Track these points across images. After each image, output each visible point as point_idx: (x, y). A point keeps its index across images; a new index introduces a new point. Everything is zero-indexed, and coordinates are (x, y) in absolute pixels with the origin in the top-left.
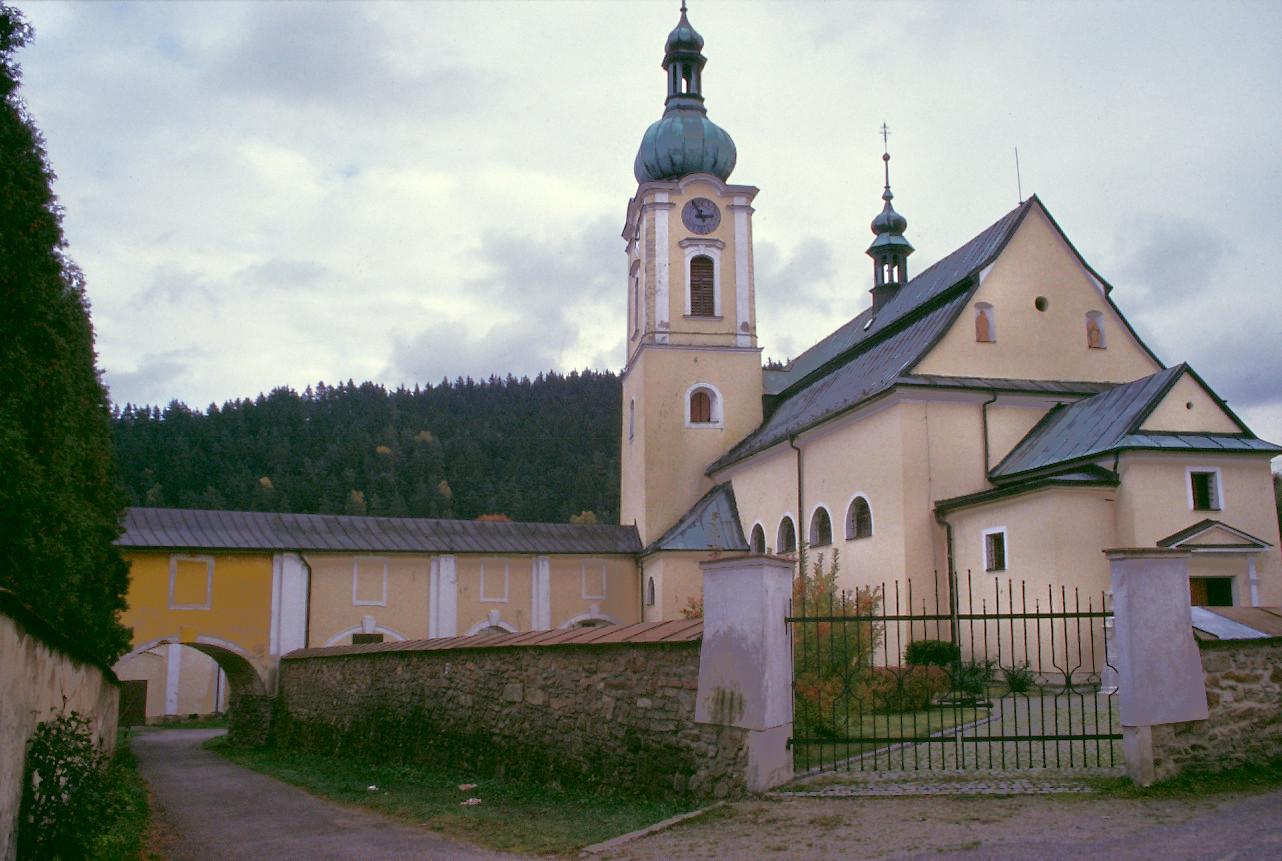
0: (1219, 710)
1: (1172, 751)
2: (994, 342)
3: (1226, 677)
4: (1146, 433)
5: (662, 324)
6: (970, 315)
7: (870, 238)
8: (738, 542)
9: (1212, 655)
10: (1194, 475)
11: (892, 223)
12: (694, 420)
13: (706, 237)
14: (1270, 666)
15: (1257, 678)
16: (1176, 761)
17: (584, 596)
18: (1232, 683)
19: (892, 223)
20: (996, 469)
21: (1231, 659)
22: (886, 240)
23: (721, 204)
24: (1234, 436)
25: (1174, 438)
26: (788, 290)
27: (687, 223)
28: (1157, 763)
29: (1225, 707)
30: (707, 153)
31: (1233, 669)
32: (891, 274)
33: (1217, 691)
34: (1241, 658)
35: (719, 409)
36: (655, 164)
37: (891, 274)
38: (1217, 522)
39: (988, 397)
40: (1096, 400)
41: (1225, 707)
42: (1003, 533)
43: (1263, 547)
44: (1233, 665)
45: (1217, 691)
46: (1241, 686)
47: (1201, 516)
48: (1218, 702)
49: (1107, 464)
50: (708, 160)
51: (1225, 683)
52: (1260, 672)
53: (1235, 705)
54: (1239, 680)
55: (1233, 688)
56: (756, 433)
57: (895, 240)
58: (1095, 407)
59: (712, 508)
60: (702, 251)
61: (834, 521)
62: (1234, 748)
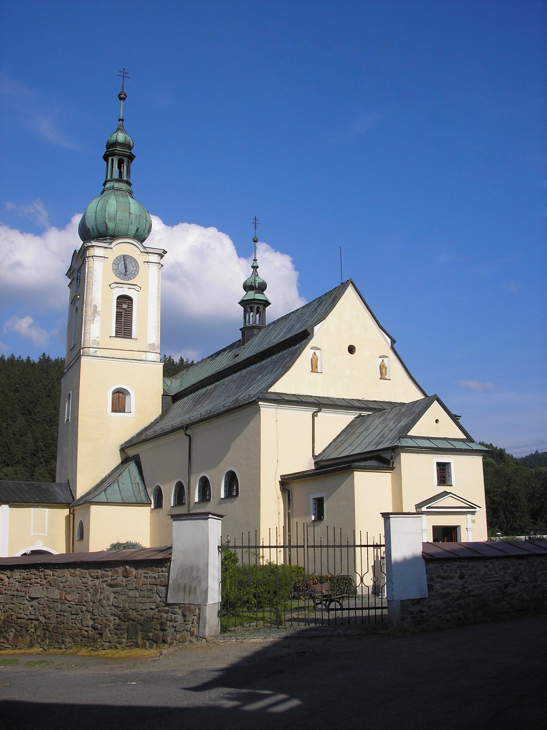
0: (433, 593)
1: (411, 613)
2: (381, 513)
3: (438, 577)
4: (412, 437)
5: (94, 341)
6: (307, 354)
7: (242, 294)
8: (144, 498)
9: (431, 566)
10: (439, 464)
11: (257, 285)
12: (114, 410)
13: (129, 282)
14: (458, 571)
15: (452, 578)
16: (412, 618)
17: (32, 534)
18: (440, 580)
19: (257, 285)
20: (320, 454)
21: (440, 568)
22: (252, 295)
23: (140, 258)
24: (462, 440)
25: (428, 441)
26: (122, 264)
27: (116, 271)
28: (403, 618)
29: (436, 592)
30: (132, 223)
31: (441, 573)
32: (254, 318)
33: (432, 584)
34: (445, 567)
35: (132, 402)
36: (94, 227)
37: (254, 318)
38: (451, 493)
39: (316, 409)
40: (383, 414)
41: (436, 592)
42: (323, 497)
43: (476, 508)
44: (441, 571)
45: (432, 584)
46: (444, 581)
47: (443, 489)
48: (433, 589)
49: (387, 456)
50: (133, 229)
51: (437, 580)
52: (453, 574)
53: (441, 591)
54: (443, 578)
55: (440, 582)
56: (157, 421)
57: (258, 296)
58: (382, 418)
59: (126, 474)
60: (125, 291)
61: (241, 490)
62: (440, 611)
